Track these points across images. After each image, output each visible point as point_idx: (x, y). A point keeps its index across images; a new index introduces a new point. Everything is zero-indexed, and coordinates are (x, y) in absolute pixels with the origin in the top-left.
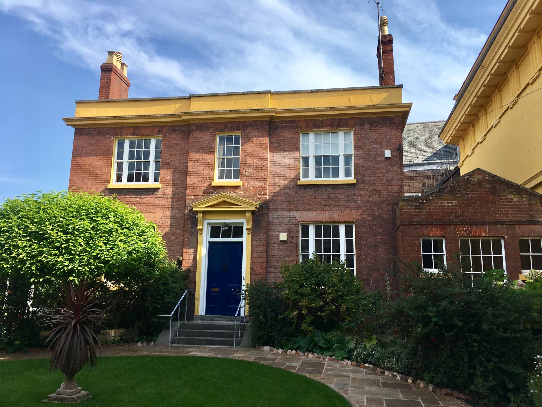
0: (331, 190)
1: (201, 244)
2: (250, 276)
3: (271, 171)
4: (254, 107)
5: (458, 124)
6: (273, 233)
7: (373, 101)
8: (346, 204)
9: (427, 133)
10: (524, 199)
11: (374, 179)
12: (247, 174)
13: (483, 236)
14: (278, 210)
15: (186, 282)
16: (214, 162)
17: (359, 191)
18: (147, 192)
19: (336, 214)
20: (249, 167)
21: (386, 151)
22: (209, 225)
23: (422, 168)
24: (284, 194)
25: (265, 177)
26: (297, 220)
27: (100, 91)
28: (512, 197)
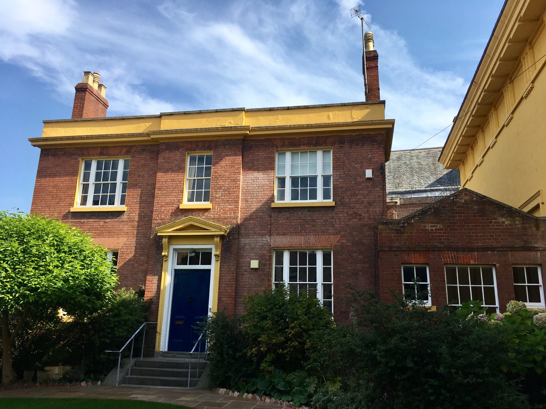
0: (308, 213)
1: (166, 270)
2: (218, 307)
3: (244, 193)
4: (227, 125)
5: (456, 146)
6: (244, 260)
7: (354, 117)
8: (324, 228)
9: (430, 159)
10: (517, 222)
11: (354, 201)
12: (218, 196)
13: (471, 263)
14: (250, 234)
15: (147, 314)
16: (184, 184)
17: (338, 214)
18: (111, 215)
19: (312, 239)
20: (220, 188)
21: (367, 171)
22: (176, 251)
23: (424, 195)
24: (257, 218)
25: (237, 199)
26: (270, 245)
27: (73, 111)
28: (504, 220)
